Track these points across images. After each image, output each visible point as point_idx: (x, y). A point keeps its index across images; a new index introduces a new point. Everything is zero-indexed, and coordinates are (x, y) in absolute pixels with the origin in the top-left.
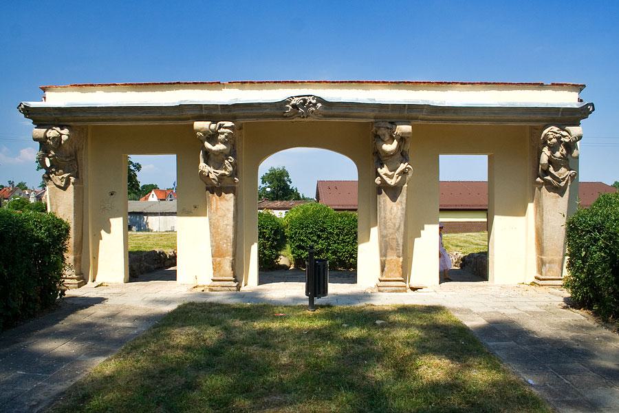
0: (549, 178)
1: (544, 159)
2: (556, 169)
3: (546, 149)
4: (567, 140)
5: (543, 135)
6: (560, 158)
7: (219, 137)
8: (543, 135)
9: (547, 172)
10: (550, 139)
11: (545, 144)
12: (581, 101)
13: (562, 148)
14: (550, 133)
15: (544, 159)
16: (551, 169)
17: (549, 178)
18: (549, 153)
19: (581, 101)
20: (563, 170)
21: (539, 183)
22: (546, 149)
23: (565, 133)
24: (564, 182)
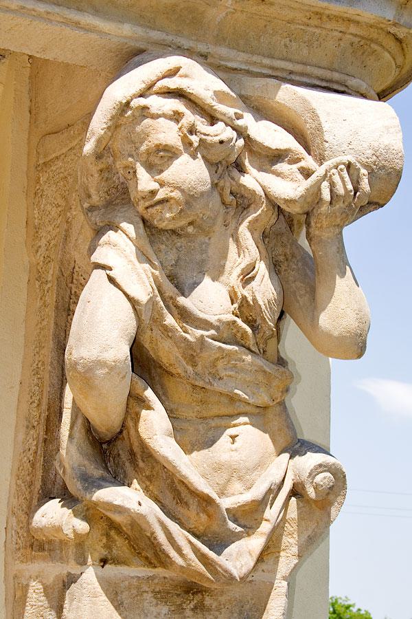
0: (129, 497)
1: (103, 328)
2: (197, 433)
3: (119, 250)
4: (286, 186)
5: (99, 123)
6: (228, 334)
7: (137, 129)
8: (99, 123)
9: (114, 452)
10: (161, 157)
11: (117, 200)
12: (140, 504)
13: (244, 250)
14: (155, 103)
15: (103, 328)
16: (155, 426)
17: (129, 497)
18: (140, 281)
19: (140, 504)
20: (245, 441)
21: (41, 545)
22: (119, 250)
23: (270, 135)
24: (255, 543)
